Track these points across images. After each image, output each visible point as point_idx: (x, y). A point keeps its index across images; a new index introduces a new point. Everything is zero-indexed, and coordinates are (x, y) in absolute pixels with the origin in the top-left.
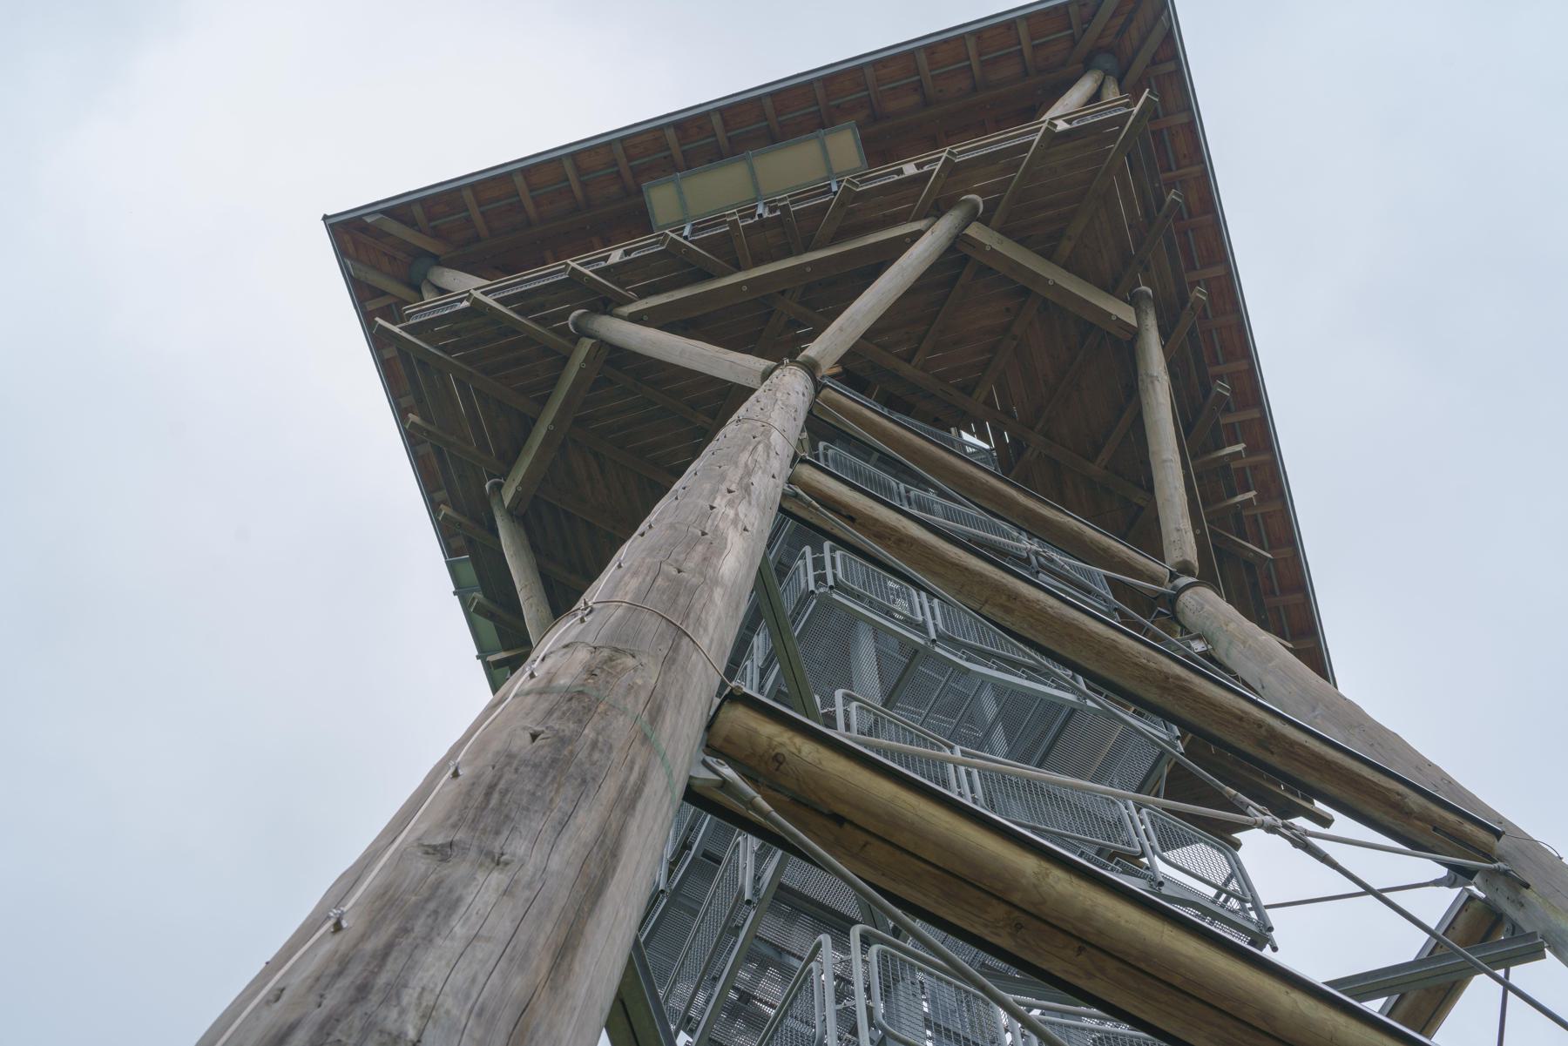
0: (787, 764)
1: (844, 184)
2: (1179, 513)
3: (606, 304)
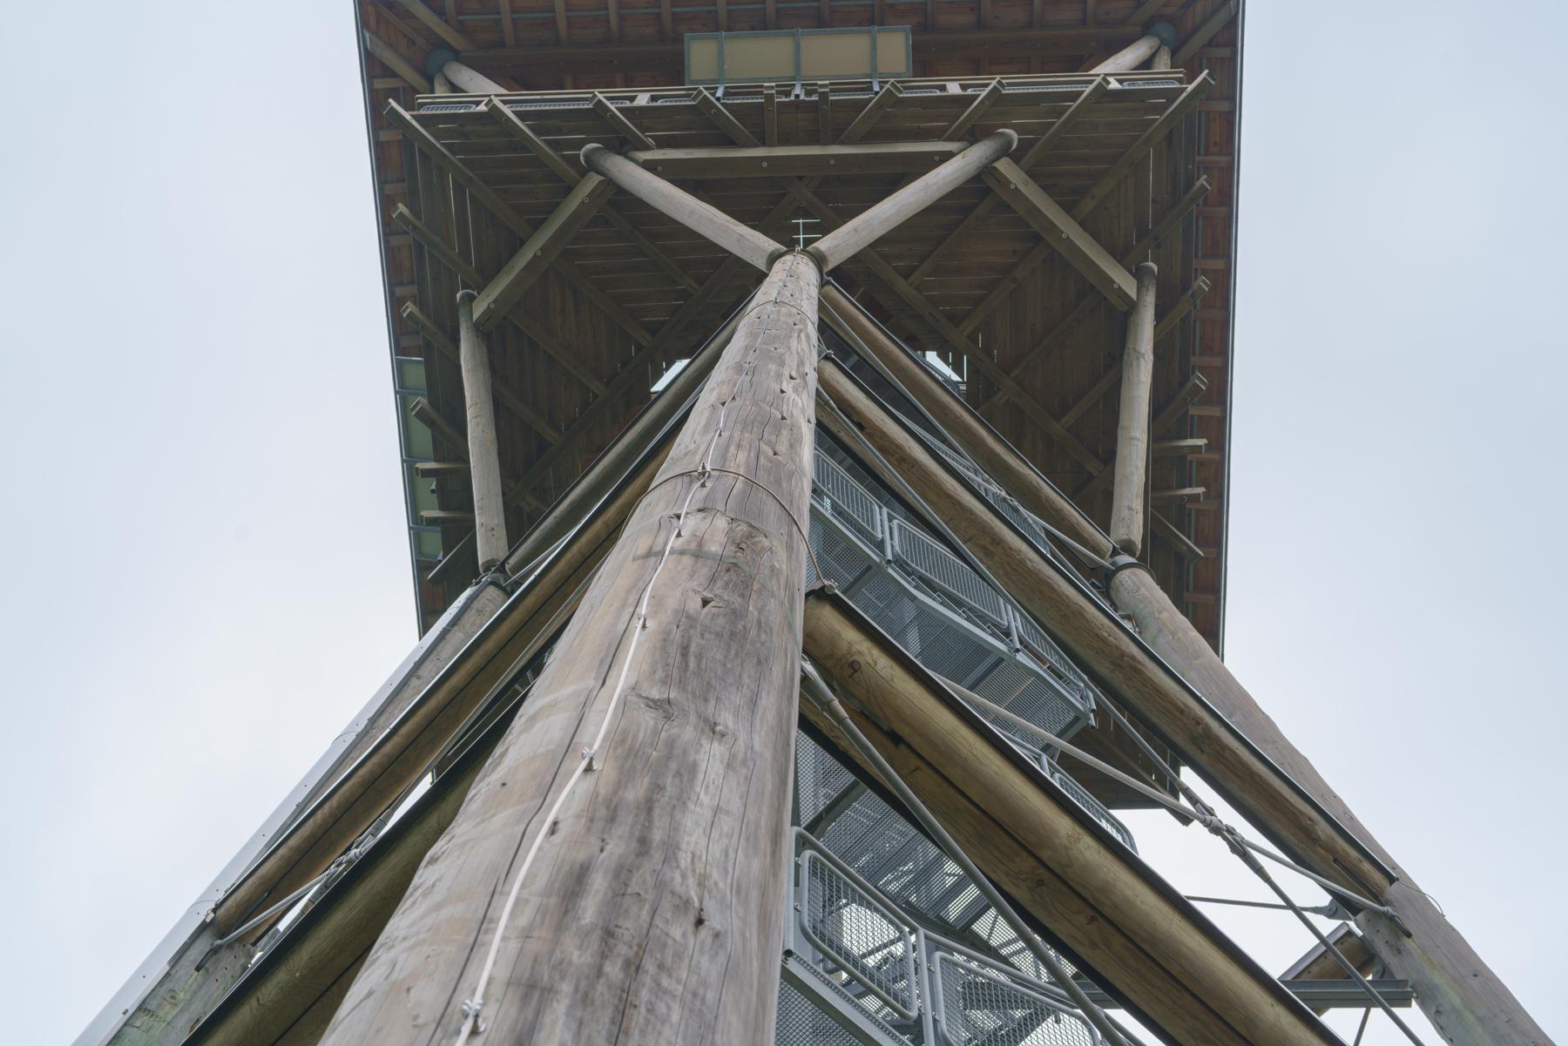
0: (862, 673)
1: (888, 86)
2: (1135, 493)
3: (623, 145)
